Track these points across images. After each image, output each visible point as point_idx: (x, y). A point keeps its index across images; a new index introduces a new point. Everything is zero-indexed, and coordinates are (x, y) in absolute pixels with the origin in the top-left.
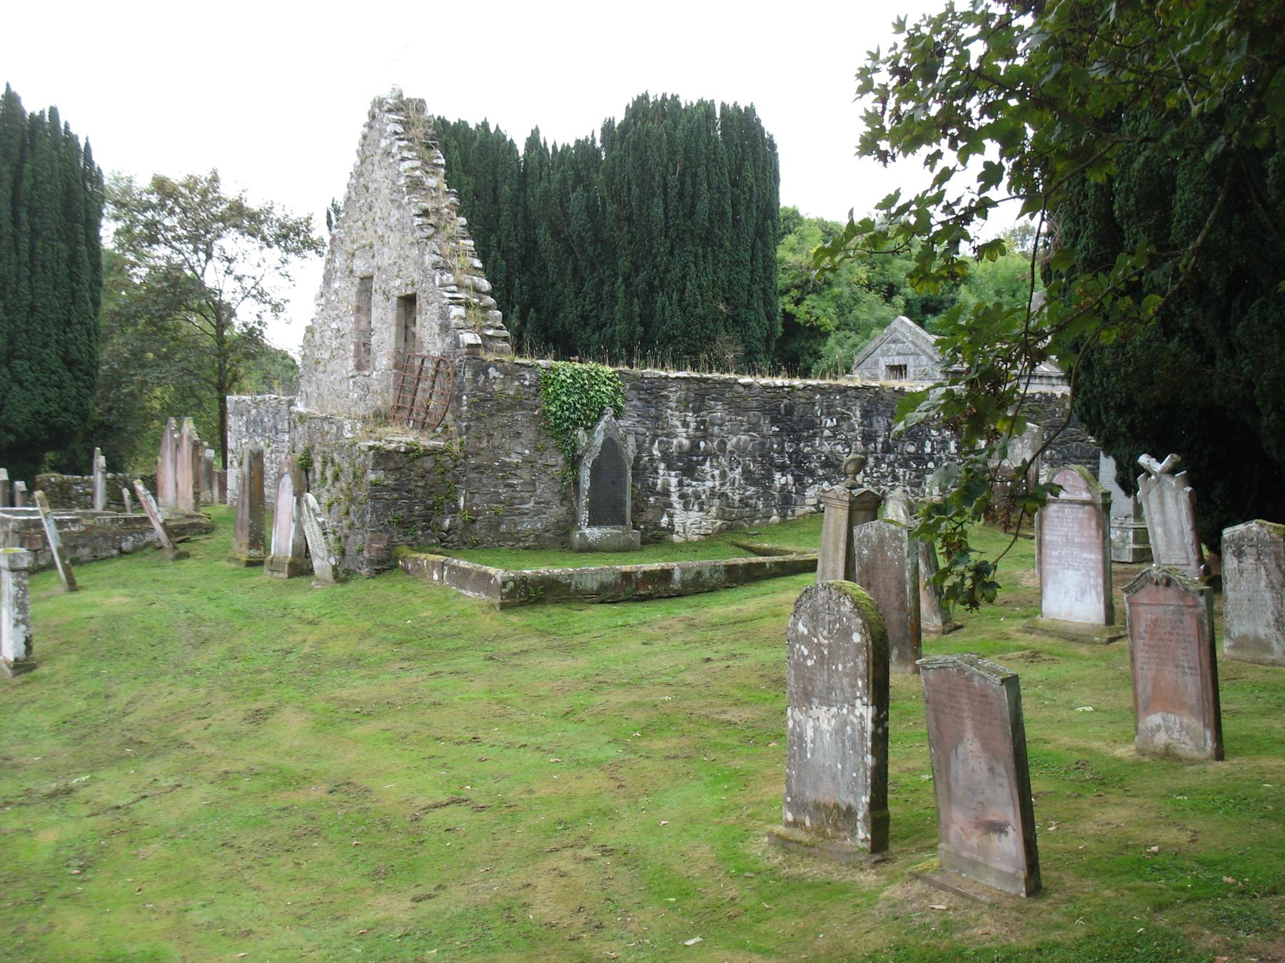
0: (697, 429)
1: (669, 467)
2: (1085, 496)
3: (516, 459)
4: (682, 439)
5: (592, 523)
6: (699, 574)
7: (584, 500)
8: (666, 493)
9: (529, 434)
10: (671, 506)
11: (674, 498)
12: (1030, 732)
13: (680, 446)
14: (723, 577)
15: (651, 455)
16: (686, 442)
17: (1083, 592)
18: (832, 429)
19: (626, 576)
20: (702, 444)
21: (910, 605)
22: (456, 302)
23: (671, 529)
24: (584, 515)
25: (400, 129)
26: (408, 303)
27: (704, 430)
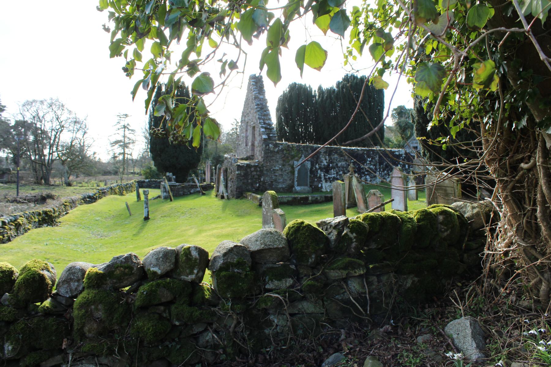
0: (329, 160)
1: (321, 171)
2: (400, 175)
3: (277, 168)
4: (325, 163)
5: (298, 185)
6: (317, 198)
7: (296, 179)
8: (320, 177)
9: (281, 162)
10: (321, 181)
11: (323, 179)
12: (16, 192)
13: (324, 165)
14: (324, 199)
15: (316, 168)
16: (326, 164)
17: (400, 202)
18: (370, 161)
19: (295, 198)
20: (331, 165)
21: (343, 204)
22: (262, 127)
23: (322, 187)
24: (296, 183)
25: (254, 83)
26: (254, 128)
27: (331, 162)
